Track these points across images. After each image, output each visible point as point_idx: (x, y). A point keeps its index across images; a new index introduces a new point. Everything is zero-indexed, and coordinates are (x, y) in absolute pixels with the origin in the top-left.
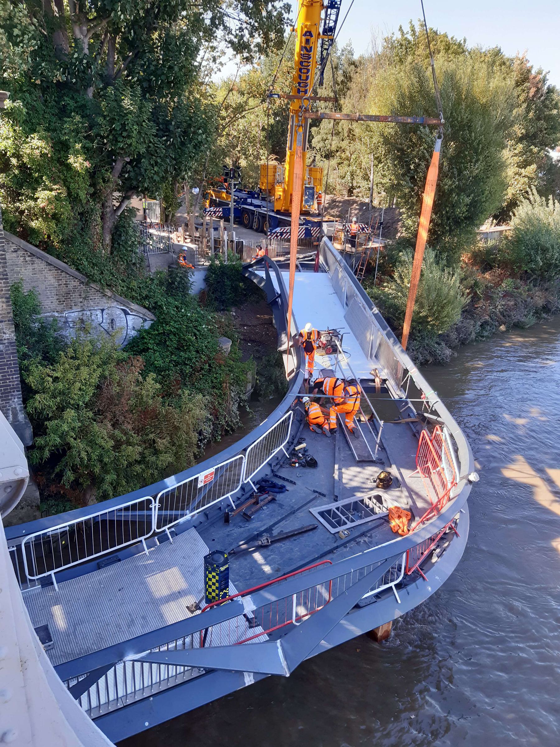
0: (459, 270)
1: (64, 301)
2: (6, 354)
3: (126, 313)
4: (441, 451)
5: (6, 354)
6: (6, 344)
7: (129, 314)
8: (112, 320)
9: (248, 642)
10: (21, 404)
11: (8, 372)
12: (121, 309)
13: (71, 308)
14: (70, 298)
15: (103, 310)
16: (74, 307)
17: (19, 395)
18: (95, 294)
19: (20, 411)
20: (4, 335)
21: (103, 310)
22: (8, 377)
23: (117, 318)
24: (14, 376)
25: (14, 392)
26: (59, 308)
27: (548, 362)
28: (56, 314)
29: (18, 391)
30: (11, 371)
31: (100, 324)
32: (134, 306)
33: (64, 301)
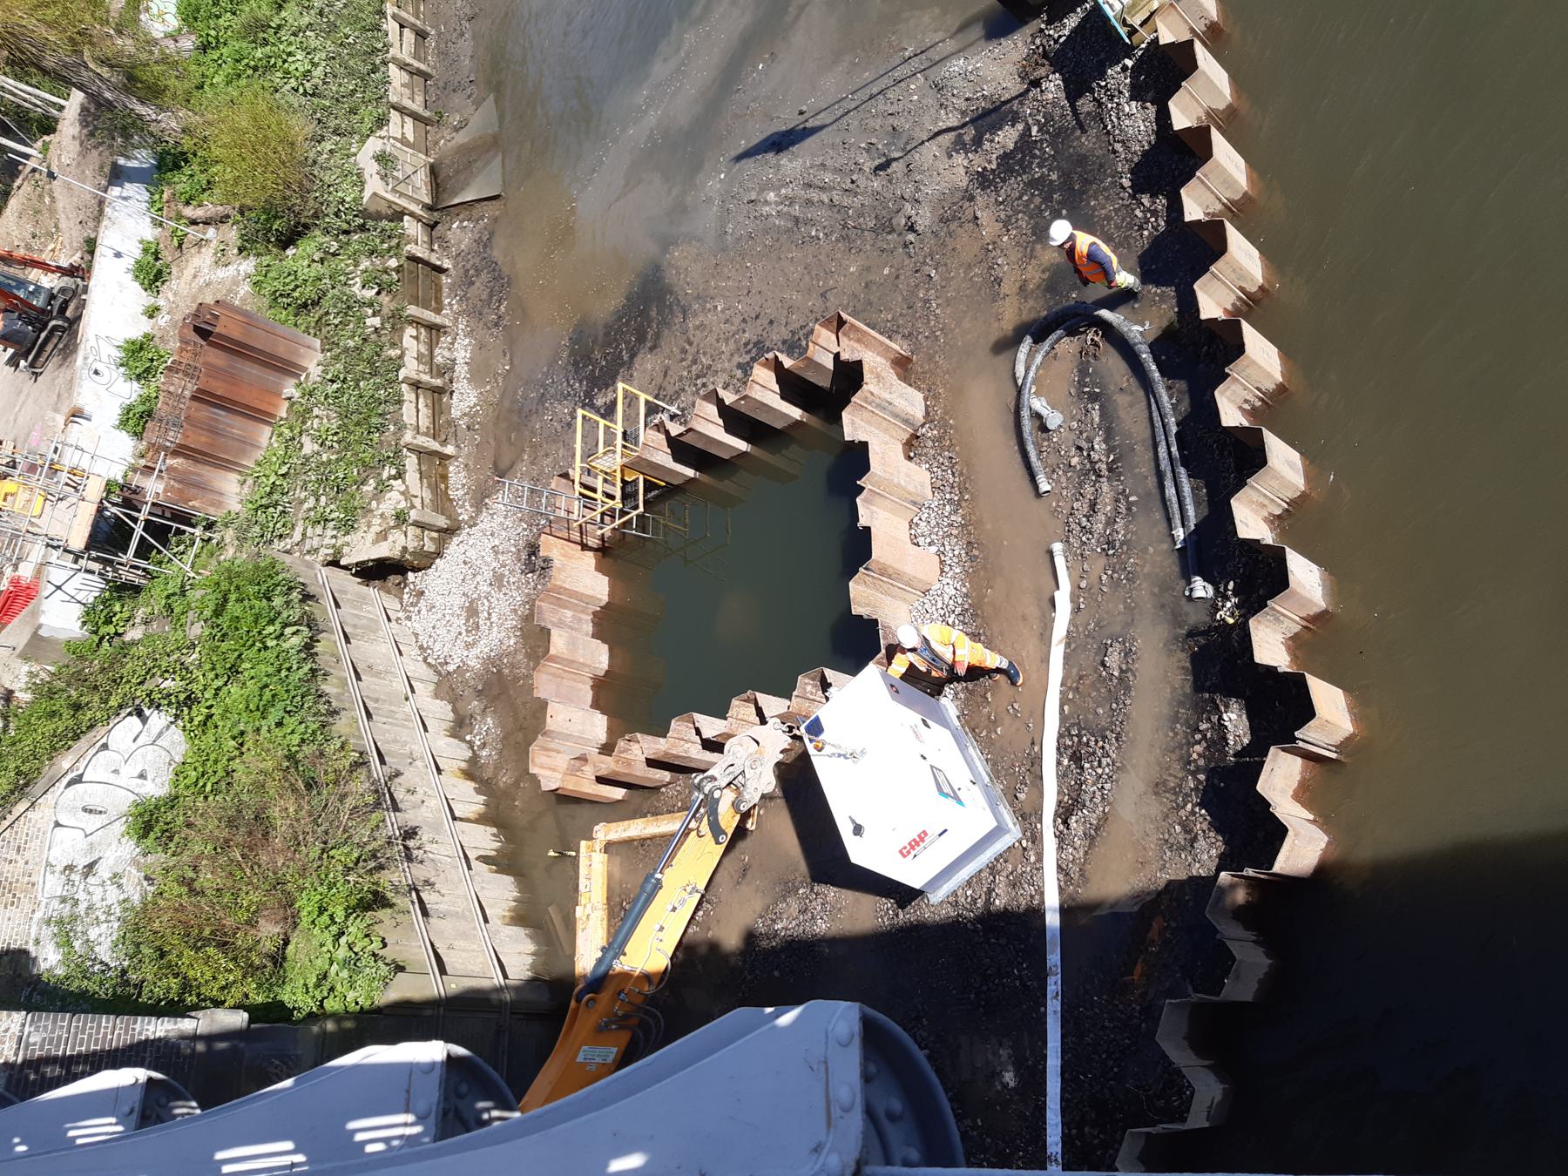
0: (376, 521)
1: (14, 895)
2: (53, 1031)
3: (78, 780)
4: (548, 1100)
5: (53, 1031)
6: (32, 1029)
7: (82, 775)
8: (85, 810)
9: (1152, 400)
10: (163, 1022)
11: (90, 1035)
12: (66, 788)
13: (33, 885)
14: (11, 883)
15: (57, 824)
16: (33, 879)
17: (143, 1021)
18: (17, 832)
19: (176, 1023)
20: (11, 1031)
21: (57, 824)
22: (101, 1036)
23: (82, 799)
24: (103, 1024)
25: (134, 1029)
26: (26, 906)
27: (421, 213)
28: (38, 915)
29: (135, 1023)
30: (91, 1028)
31: (86, 836)
32: (65, 762)
33: (14, 895)
